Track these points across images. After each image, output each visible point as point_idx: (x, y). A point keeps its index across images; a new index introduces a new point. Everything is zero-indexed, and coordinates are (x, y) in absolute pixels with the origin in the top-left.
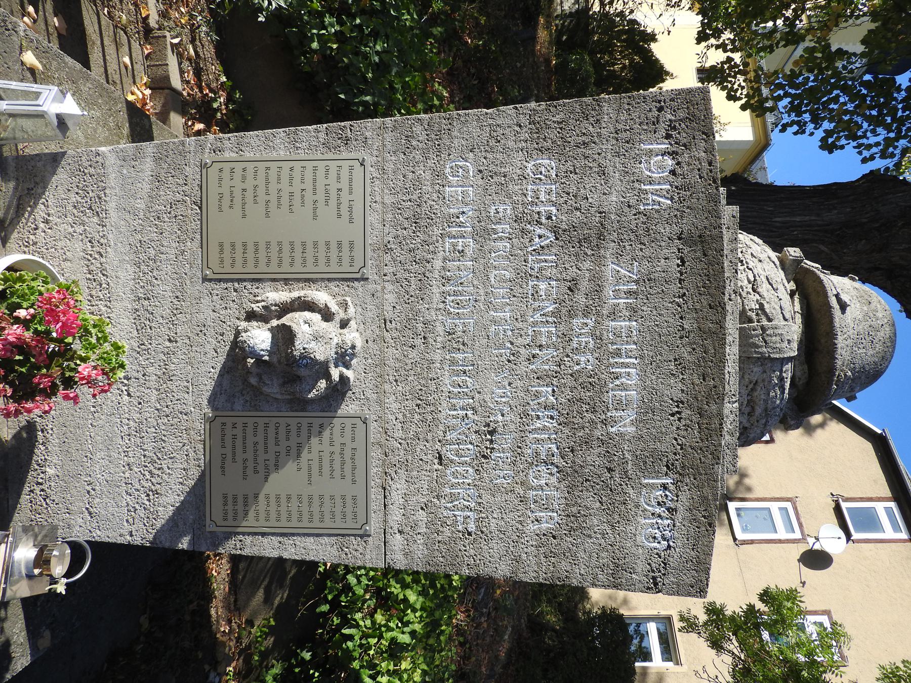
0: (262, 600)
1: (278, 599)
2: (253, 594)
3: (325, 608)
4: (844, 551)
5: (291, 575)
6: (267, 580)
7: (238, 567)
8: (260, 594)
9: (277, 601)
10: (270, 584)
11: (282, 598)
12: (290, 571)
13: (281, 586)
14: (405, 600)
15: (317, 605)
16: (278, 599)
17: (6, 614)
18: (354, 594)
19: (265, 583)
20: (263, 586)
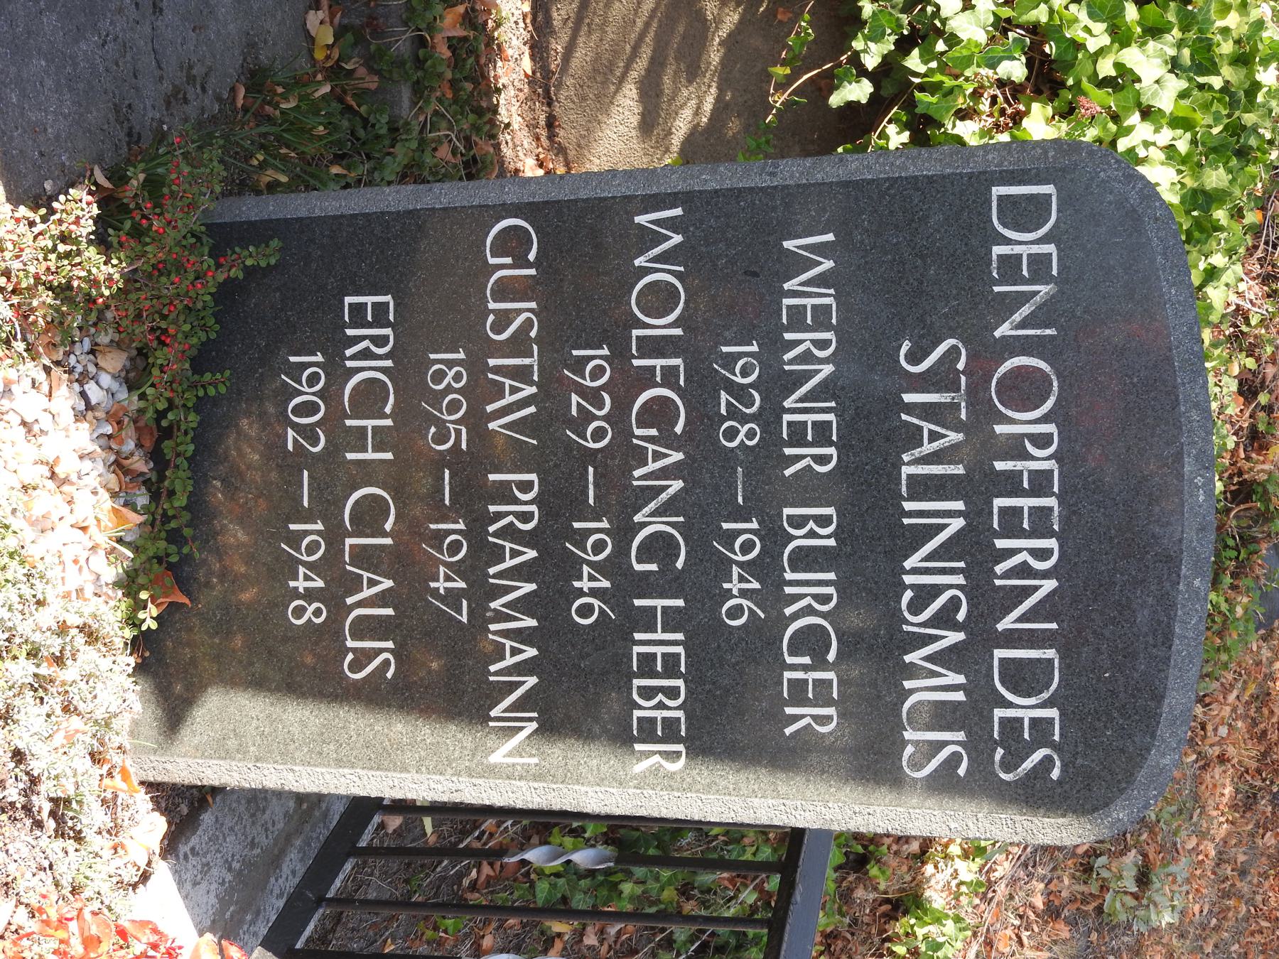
0: (634, 120)
1: (687, 113)
2: (604, 102)
3: (860, 91)
4: (169, 823)
5: (723, 32)
6: (646, 52)
7: (548, 19)
8: (628, 104)
9: (681, 127)
10: (657, 65)
11: (697, 112)
12: (718, 21)
13: (693, 72)
14: (1123, 80)
15: (829, 83)
16: (687, 113)
17: (648, 731)
18: (953, 40)
19: (641, 64)
20: (634, 74)
